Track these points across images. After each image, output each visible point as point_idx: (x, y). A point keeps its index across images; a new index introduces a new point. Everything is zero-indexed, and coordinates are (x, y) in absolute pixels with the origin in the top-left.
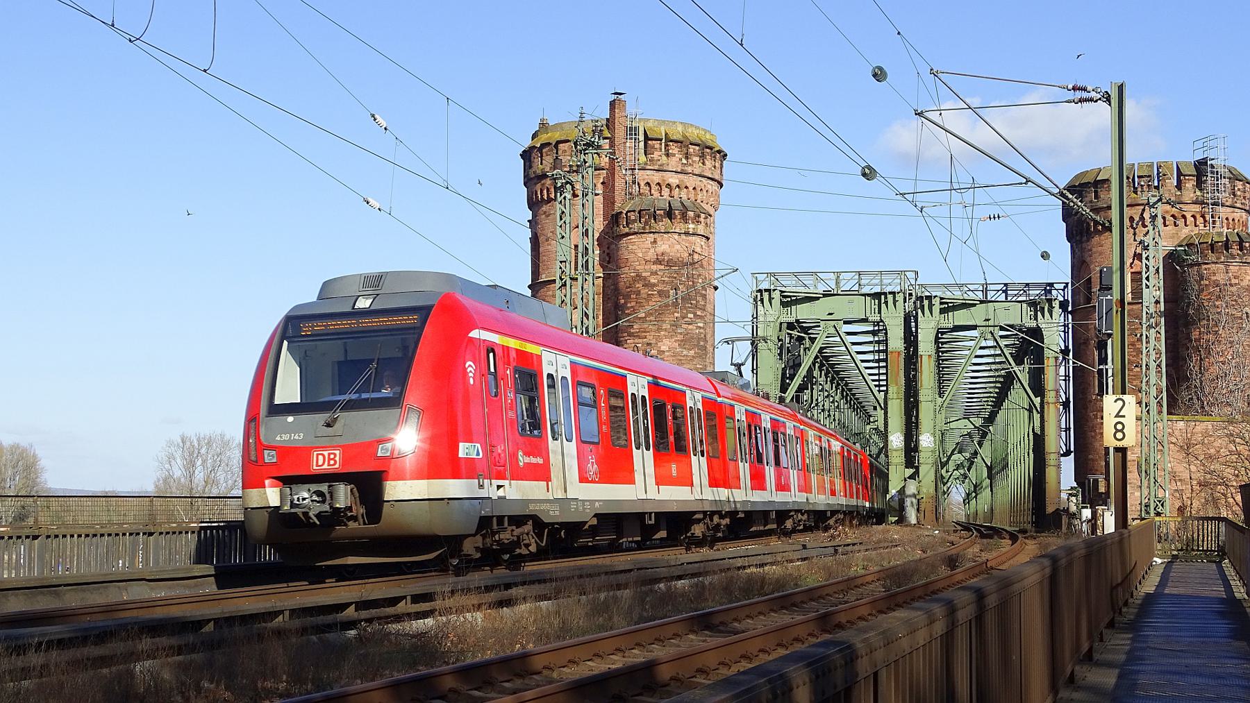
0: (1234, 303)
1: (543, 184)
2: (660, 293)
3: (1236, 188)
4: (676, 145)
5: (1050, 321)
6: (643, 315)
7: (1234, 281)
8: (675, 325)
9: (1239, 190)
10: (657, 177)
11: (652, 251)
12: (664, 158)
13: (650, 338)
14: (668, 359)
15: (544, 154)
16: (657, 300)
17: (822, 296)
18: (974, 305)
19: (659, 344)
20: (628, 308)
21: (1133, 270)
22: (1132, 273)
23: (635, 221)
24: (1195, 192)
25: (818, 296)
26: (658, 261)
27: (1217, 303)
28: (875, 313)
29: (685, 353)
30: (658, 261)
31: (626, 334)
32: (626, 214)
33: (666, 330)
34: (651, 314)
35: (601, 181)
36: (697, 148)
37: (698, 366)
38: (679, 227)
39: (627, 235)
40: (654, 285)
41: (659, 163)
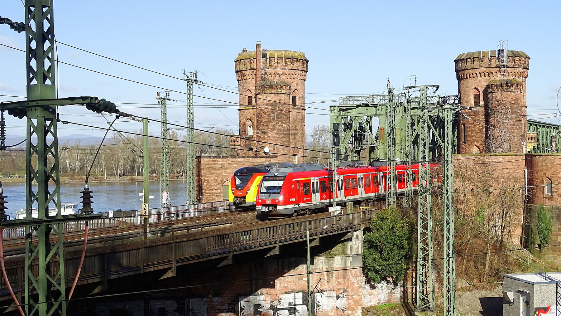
0: (504, 108)
2: (268, 115)
3: (515, 60)
4: (280, 59)
7: (504, 99)
8: (274, 127)
9: (517, 60)
10: (274, 71)
12: (276, 64)
16: (267, 118)
21: (474, 94)
24: (496, 63)
25: (354, 107)
26: (267, 104)
27: (498, 108)
29: (278, 136)
30: (267, 104)
34: (265, 123)
35: (254, 74)
36: (290, 59)
37: (283, 141)
38: (275, 91)
40: (266, 113)
41: (274, 66)
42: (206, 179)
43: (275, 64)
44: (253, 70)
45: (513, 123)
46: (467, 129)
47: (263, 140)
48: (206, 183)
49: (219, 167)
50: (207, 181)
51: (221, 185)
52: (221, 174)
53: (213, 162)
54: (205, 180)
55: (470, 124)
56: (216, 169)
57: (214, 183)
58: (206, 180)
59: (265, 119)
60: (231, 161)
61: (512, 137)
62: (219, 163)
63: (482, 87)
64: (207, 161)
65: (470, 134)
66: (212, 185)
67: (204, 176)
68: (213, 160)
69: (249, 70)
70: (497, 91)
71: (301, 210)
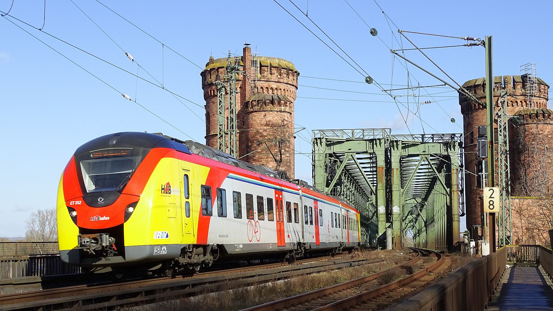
0: (541, 142)
3: (541, 88)
4: (275, 69)
5: (454, 152)
6: (260, 151)
7: (540, 132)
10: (266, 84)
11: (264, 120)
12: (270, 75)
13: (263, 162)
23: (256, 105)
26: (267, 125)
27: (533, 143)
30: (267, 125)
32: (251, 102)
35: (239, 86)
36: (285, 70)
38: (277, 108)
39: (252, 112)
41: (267, 77)
43: (268, 74)
44: (238, 81)
45: (550, 161)
61: (550, 178)
70: (531, 122)
71: (228, 279)
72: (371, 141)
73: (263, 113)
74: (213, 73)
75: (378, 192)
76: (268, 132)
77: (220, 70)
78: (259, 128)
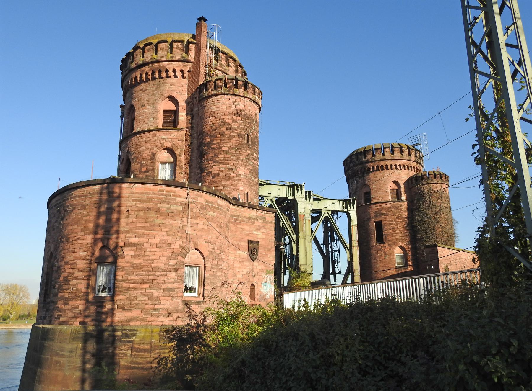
1: (143, 71)
2: (239, 135)
5: (353, 209)
6: (226, 149)
11: (234, 107)
13: (231, 165)
14: (244, 180)
15: (146, 51)
17: (266, 184)
18: (320, 200)
19: (238, 170)
20: (214, 144)
21: (391, 188)
22: (391, 189)
23: (221, 86)
26: (237, 114)
28: (291, 195)
29: (253, 179)
30: (237, 114)
31: (212, 162)
32: (215, 82)
33: (242, 160)
34: (233, 148)
39: (215, 95)
40: (235, 129)
42: (133, 240)
44: (187, 62)
46: (386, 227)
47: (226, 180)
48: (132, 253)
49: (179, 211)
50: (139, 247)
51: (180, 258)
52: (181, 230)
53: (162, 195)
54: (128, 244)
55: (390, 221)
56: (168, 213)
57: (161, 254)
58: (135, 245)
59: (232, 141)
60: (207, 201)
62: (179, 200)
63: (402, 181)
64: (143, 191)
65: (391, 233)
66: (154, 258)
67: (127, 232)
68: (160, 190)
69: (179, 61)
72: (292, 186)
73: (233, 98)
74: (147, 50)
75: (300, 240)
76: (238, 125)
77: (160, 45)
78: (227, 117)
